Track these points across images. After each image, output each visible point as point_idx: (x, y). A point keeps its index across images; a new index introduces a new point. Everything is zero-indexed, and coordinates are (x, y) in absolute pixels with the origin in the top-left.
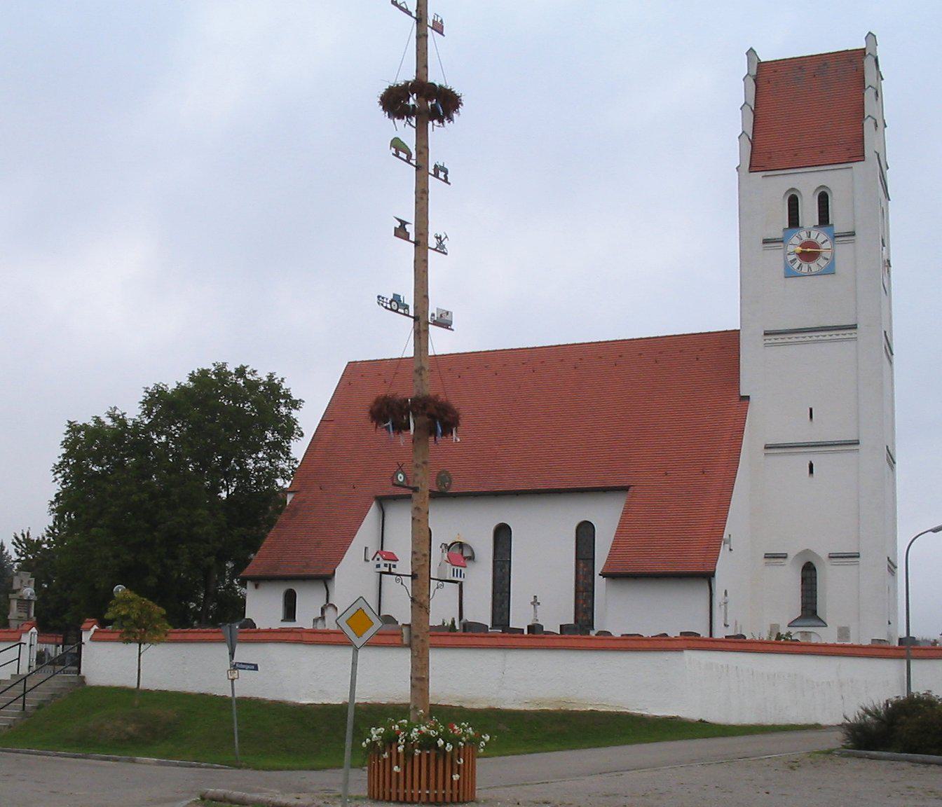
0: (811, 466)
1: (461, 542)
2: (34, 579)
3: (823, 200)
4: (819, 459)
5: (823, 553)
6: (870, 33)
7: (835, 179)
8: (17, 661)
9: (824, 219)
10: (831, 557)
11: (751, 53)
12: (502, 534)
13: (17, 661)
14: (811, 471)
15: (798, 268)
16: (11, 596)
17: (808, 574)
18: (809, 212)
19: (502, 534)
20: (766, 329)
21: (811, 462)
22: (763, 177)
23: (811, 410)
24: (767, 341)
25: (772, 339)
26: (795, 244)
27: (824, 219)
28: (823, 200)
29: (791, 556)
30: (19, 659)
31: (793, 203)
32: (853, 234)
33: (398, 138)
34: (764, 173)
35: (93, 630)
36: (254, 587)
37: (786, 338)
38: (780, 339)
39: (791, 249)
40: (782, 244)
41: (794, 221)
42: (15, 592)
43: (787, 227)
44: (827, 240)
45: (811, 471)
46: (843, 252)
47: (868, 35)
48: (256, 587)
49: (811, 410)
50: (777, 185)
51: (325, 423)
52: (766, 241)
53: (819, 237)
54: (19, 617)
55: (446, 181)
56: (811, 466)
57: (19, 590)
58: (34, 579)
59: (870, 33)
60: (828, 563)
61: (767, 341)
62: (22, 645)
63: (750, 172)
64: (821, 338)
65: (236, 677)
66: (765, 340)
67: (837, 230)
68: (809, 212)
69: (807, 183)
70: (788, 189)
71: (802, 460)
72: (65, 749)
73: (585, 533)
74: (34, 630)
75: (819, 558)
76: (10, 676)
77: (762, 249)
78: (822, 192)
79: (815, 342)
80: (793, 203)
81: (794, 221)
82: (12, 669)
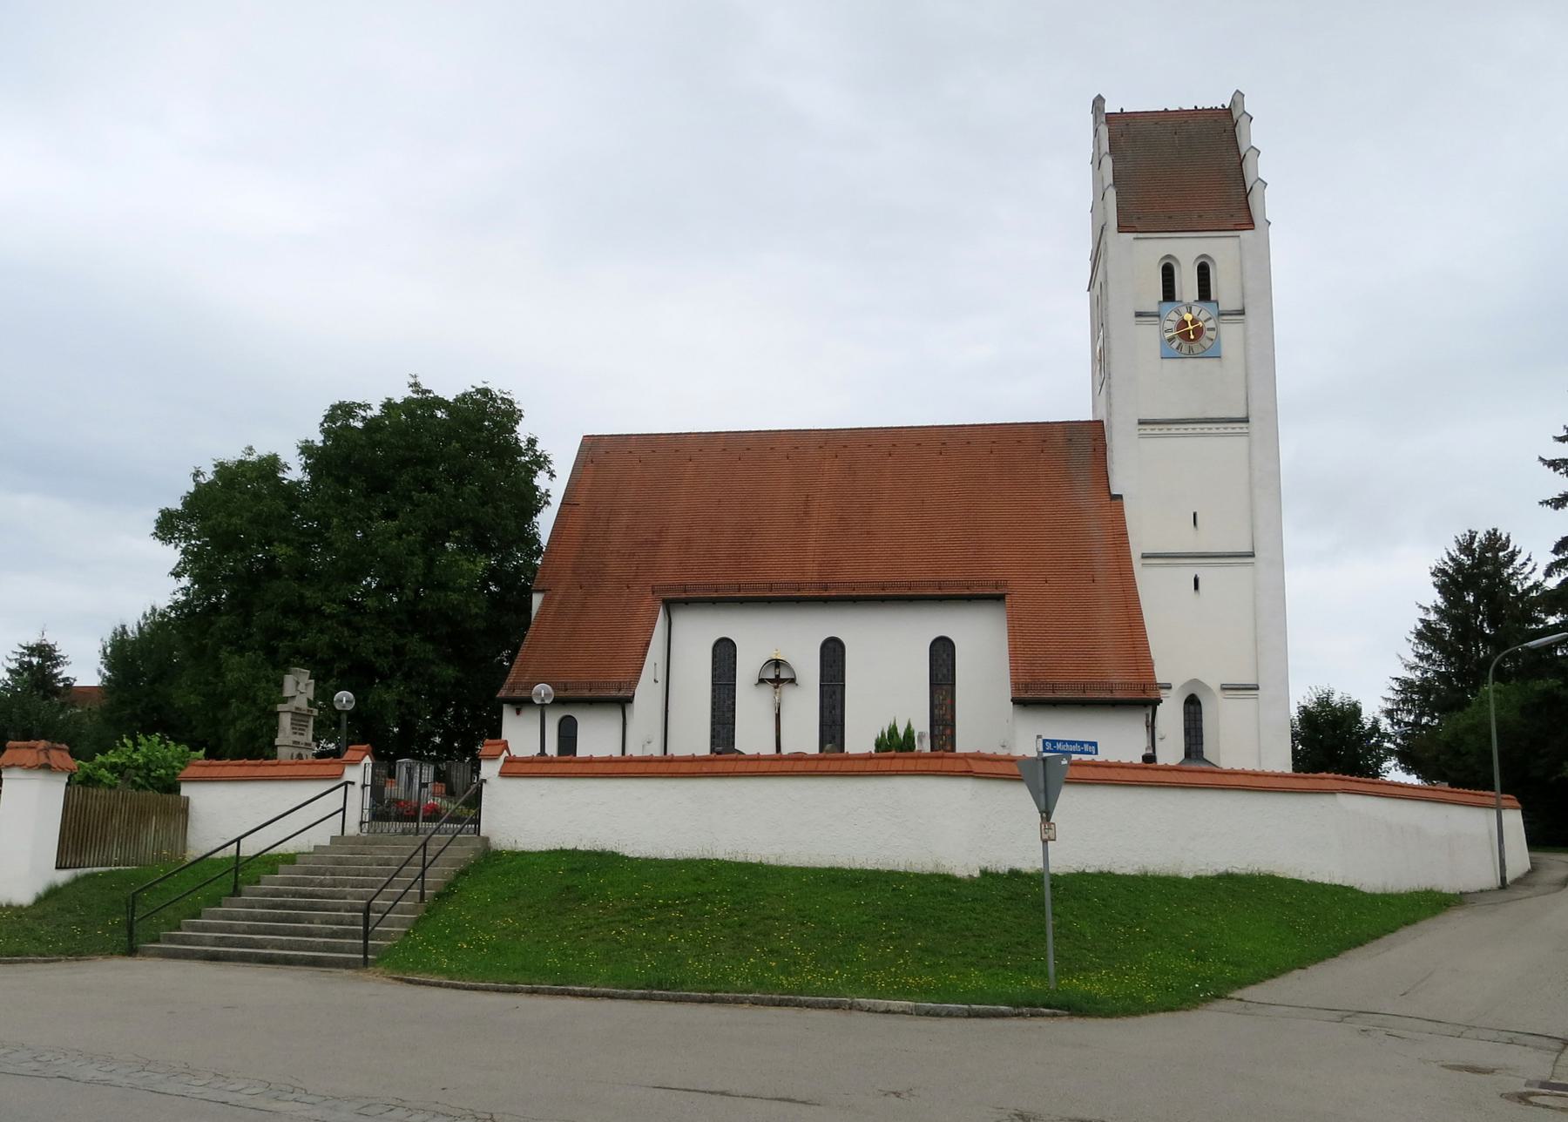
0: (1196, 581)
1: (777, 660)
2: (313, 681)
3: (1204, 272)
4: (1208, 574)
5: (1215, 685)
6: (1237, 91)
7: (1220, 248)
8: (341, 813)
9: (1204, 293)
10: (1225, 688)
11: (1098, 102)
12: (833, 654)
13: (341, 813)
14: (1196, 587)
15: (1177, 348)
16: (280, 707)
17: (1192, 707)
18: (1187, 284)
19: (833, 654)
20: (1141, 418)
21: (1196, 576)
22: (1135, 239)
23: (1195, 515)
24: (1142, 432)
25: (1148, 429)
26: (1172, 317)
27: (1204, 293)
28: (1204, 272)
29: (1176, 687)
30: (344, 809)
31: (1168, 273)
32: (1242, 312)
33: (734, 645)
34: (1135, 235)
35: (502, 758)
36: (629, 704)
37: (1165, 429)
38: (1157, 429)
39: (1169, 325)
40: (1157, 319)
41: (1169, 293)
42: (285, 701)
43: (1162, 299)
44: (1210, 318)
45: (1196, 587)
46: (1230, 333)
47: (1235, 93)
48: (518, 713)
49: (1195, 515)
50: (1150, 251)
51: (569, 507)
52: (1139, 315)
53: (1203, 313)
54: (295, 742)
55: (761, 681)
56: (1196, 581)
57: (293, 697)
58: (313, 681)
59: (1237, 91)
60: (1220, 695)
61: (1142, 432)
62: (349, 785)
63: (1119, 232)
64: (1206, 431)
65: (1052, 837)
66: (1139, 430)
67: (1223, 307)
68: (1187, 284)
69: (1187, 249)
70: (1164, 255)
71: (1186, 573)
72: (308, 944)
73: (942, 653)
74: (368, 760)
75: (1207, 689)
76: (486, 835)
77: (1134, 323)
78: (1202, 263)
79: (1198, 435)
80: (1168, 273)
81: (1169, 293)
82: (333, 827)
